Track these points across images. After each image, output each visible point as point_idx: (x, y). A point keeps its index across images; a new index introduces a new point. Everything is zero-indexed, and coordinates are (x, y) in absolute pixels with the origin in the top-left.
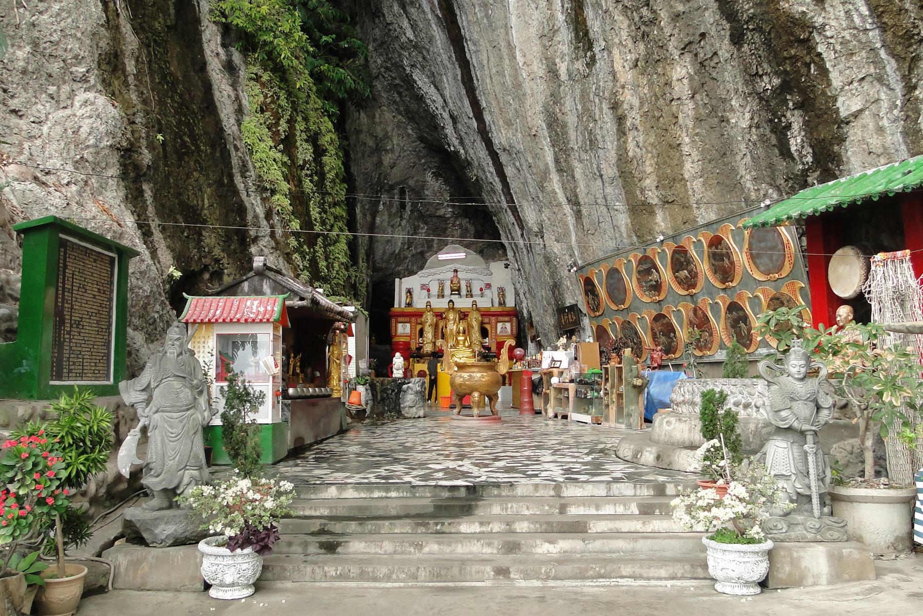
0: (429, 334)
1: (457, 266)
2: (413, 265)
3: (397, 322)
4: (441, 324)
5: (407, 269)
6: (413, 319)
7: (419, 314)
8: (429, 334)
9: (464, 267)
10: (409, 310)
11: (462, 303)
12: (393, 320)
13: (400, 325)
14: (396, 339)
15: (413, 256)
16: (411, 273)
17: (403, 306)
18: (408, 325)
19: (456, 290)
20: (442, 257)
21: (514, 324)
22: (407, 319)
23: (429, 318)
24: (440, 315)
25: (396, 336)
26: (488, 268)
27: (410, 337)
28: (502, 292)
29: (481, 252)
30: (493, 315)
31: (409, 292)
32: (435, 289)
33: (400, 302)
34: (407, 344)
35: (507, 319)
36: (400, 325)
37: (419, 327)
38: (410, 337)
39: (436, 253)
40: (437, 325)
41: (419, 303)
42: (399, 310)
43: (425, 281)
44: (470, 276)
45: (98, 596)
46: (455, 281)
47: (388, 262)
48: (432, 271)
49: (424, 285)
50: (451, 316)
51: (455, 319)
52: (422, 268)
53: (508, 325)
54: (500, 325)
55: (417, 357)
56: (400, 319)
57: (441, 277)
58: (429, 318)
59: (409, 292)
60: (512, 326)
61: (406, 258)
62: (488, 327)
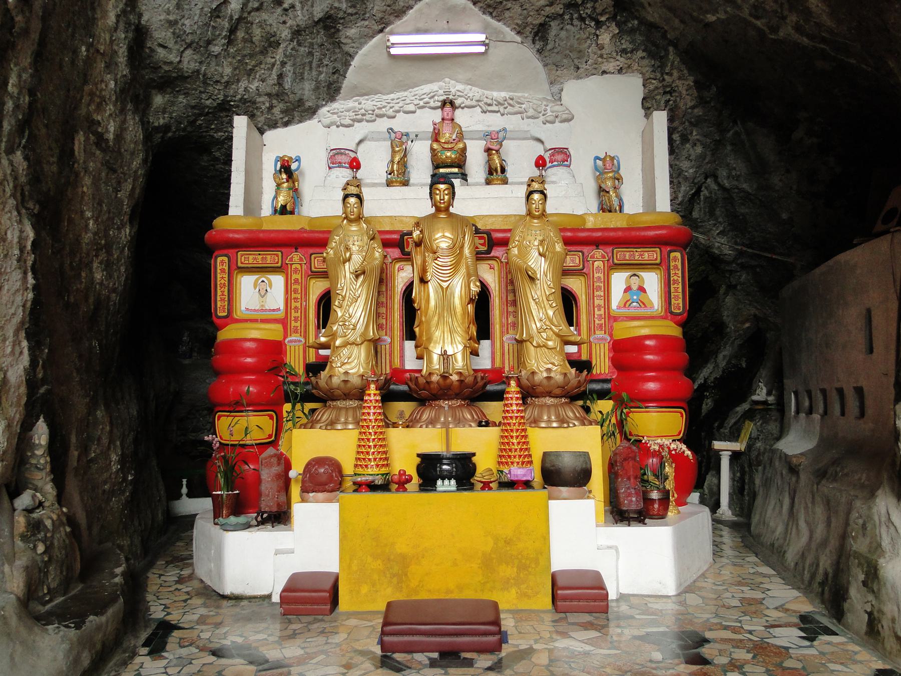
0: (354, 310)
1: (455, 88)
2: (299, 77)
3: (235, 269)
4: (403, 275)
5: (279, 95)
6: (296, 256)
7: (314, 241)
8: (354, 310)
9: (475, 92)
10: (285, 224)
11: (477, 201)
12: (221, 263)
13: (247, 284)
14: (226, 334)
15: (297, 33)
16: (297, 111)
17: (266, 210)
18: (278, 281)
19: (447, 171)
20: (404, 41)
21: (677, 275)
22: (271, 258)
23: (356, 250)
24: (399, 243)
25: (230, 318)
26: (557, 98)
27: (284, 322)
28: (608, 174)
29: (539, 35)
30: (597, 243)
31: (286, 169)
32: (376, 162)
33: (249, 199)
34: (273, 350)
35: (651, 255)
36: (247, 284)
37: (317, 288)
38: (284, 322)
39: (383, 25)
40: (383, 280)
41: (321, 201)
42: (248, 224)
43: (345, 139)
44: (495, 122)
45: (641, 149)
46: (447, 134)
47: (201, 46)
48: (368, 103)
49: (338, 152)
50: (443, 239)
51: (456, 249)
52: (332, 91)
53: (652, 281)
54: (619, 280)
55: (308, 397)
56: (247, 258)
57: (401, 124)
58: (356, 250)
59: (286, 169)
60: (667, 284)
61: (272, 42)
62: (576, 285)
